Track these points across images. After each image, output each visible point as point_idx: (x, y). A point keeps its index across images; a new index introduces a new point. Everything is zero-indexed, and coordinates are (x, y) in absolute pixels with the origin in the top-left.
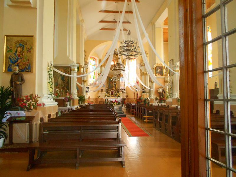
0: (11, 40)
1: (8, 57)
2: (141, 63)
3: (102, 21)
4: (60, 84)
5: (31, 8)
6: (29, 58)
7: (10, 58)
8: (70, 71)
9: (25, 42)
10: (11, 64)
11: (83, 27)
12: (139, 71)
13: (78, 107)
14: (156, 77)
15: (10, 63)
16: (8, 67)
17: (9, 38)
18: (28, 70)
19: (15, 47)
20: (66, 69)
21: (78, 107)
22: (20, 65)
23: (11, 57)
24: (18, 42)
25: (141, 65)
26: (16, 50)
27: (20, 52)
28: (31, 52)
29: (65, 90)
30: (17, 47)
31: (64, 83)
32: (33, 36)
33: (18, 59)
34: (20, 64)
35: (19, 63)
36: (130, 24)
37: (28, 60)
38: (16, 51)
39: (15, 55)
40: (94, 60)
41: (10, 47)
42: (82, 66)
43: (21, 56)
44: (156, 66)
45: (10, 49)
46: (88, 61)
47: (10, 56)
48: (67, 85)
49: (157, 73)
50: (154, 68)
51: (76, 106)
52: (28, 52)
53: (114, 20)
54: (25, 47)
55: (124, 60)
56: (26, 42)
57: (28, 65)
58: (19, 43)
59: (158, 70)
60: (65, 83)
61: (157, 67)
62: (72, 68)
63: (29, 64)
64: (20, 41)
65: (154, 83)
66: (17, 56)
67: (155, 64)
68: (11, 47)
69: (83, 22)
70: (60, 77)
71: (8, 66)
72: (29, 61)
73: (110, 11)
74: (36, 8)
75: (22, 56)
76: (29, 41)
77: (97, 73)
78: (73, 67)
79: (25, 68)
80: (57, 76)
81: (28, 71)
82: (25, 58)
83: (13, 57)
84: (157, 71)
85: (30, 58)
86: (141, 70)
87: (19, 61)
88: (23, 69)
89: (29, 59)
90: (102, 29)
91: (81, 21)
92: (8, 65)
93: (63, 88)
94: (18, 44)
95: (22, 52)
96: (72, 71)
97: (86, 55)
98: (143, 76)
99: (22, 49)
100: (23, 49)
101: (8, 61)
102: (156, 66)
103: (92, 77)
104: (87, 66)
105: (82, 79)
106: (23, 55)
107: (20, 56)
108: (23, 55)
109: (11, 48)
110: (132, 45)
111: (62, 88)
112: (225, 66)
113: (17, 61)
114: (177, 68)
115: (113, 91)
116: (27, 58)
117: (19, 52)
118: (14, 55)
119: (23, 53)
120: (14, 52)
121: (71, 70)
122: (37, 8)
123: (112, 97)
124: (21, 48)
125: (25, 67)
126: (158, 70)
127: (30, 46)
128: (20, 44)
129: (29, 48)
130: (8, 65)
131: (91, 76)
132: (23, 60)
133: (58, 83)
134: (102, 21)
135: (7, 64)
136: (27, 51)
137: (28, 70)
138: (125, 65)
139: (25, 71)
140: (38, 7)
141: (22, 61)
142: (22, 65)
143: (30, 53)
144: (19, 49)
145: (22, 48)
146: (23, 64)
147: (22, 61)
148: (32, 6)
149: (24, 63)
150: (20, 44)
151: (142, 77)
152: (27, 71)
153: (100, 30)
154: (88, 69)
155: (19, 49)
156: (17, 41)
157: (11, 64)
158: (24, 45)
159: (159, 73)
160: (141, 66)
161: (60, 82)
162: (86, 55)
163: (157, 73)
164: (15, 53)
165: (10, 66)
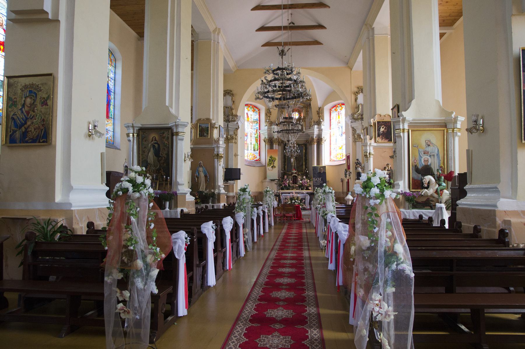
0: (16, 85)
1: (11, 117)
2: (353, 115)
3: (263, 29)
4: (152, 163)
5: (48, 21)
6: (45, 117)
7: (13, 119)
8: (170, 136)
9: (38, 86)
10: (15, 129)
11: (218, 42)
12: (351, 129)
13: (226, 205)
14: (375, 144)
15: (13, 128)
16: (11, 136)
17: (12, 80)
18: (43, 140)
19: (22, 98)
20: (163, 133)
21: (226, 205)
22: (30, 131)
23: (15, 117)
24: (26, 87)
25: (354, 118)
26: (23, 102)
27: (29, 106)
28: (48, 105)
29: (162, 175)
30: (25, 98)
31: (159, 161)
32: (50, 75)
33: (27, 119)
34: (30, 130)
35: (29, 127)
36: (256, 29)
37: (43, 120)
38: (23, 105)
39: (22, 112)
40: (254, 111)
41: (14, 97)
42: (215, 124)
43: (31, 113)
44: (376, 121)
45: (14, 102)
46: (238, 114)
47: (14, 115)
48: (165, 164)
49: (379, 136)
50: (371, 126)
51: (222, 204)
52: (42, 106)
53: (292, 25)
54: (38, 96)
55: (319, 110)
56: (39, 86)
57: (42, 130)
58: (28, 90)
59: (382, 130)
60: (162, 161)
61: (378, 122)
62: (175, 131)
63: (45, 127)
64: (30, 84)
65: (372, 159)
66: (25, 114)
67: (373, 117)
68: (16, 97)
69: (218, 34)
70: (152, 149)
71: (10, 134)
72: (45, 123)
73: (276, 6)
74: (58, 21)
75: (33, 114)
76: (46, 84)
77: (263, 138)
78: (177, 128)
79: (38, 135)
80: (145, 147)
81: (43, 142)
82: (38, 117)
83: (18, 115)
84: (379, 130)
85: (47, 116)
86: (354, 130)
87: (29, 123)
88: (35, 138)
89: (45, 119)
90: (267, 44)
91: (214, 31)
92: (10, 132)
93: (158, 171)
94: (26, 91)
95: (33, 105)
96: (174, 137)
97: (234, 102)
98: (357, 143)
99: (34, 100)
100: (35, 101)
101: (10, 124)
102: (377, 119)
103: (251, 148)
104: (237, 123)
105: (215, 153)
106: (34, 112)
107: (29, 113)
108: (34, 112)
109: (15, 100)
110: (288, 77)
111: (156, 173)
112: (465, 119)
113: (26, 123)
114: (403, 126)
115: (296, 176)
116: (41, 117)
117: (28, 107)
118: (20, 112)
119: (36, 108)
120: (21, 107)
121: (172, 135)
122: (60, 19)
123: (293, 188)
124: (31, 98)
125: (37, 134)
126: (382, 130)
127: (47, 93)
128: (30, 91)
129: (44, 98)
130: (10, 132)
131: (249, 145)
132: (34, 121)
133: (149, 161)
134: (263, 29)
135: (9, 130)
136: (42, 104)
137: (43, 140)
138: (323, 119)
139: (38, 141)
140: (62, 18)
141: (32, 123)
142: (33, 130)
143: (47, 107)
144: (29, 101)
145: (33, 98)
146: (35, 129)
147: (32, 123)
148: (50, 17)
149: (37, 126)
150: (31, 92)
151: (355, 145)
152: (41, 141)
153: (263, 46)
154: (239, 131)
155: (29, 101)
156: (25, 86)
157: (15, 129)
158: (36, 92)
159: (383, 136)
160: (353, 120)
161: (152, 161)
162: (234, 102)
163: (379, 136)
164: (21, 109)
165: (13, 133)
